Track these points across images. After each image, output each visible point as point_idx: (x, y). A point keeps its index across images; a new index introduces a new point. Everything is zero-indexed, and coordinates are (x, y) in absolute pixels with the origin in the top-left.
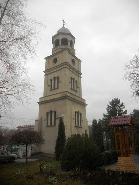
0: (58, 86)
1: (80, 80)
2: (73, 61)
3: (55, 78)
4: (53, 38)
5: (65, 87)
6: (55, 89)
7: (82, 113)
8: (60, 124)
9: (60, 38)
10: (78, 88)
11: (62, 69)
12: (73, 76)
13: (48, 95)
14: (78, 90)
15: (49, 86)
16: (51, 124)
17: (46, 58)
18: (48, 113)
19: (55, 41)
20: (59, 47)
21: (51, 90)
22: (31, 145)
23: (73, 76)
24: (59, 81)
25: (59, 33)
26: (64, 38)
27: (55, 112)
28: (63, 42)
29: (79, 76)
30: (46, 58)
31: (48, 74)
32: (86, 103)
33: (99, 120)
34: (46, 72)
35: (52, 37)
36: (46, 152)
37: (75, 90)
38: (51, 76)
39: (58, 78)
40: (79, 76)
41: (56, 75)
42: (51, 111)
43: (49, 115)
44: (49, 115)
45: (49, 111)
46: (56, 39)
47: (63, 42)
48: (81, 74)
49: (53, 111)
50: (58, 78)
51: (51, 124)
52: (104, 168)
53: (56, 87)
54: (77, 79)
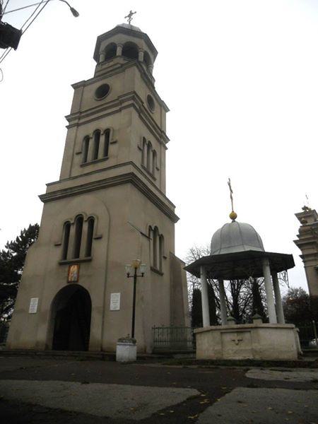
0: (89, 252)
1: (162, 154)
2: (150, 100)
4: (101, 39)
5: (125, 154)
6: (96, 159)
7: (158, 153)
8: (127, 29)
9: (121, 39)
12: (150, 138)
13: (73, 175)
14: (157, 176)
15: (78, 154)
16: (77, 254)
17: (75, 86)
20: (116, 61)
21: (85, 164)
23: (150, 138)
24: (110, 141)
25: (119, 30)
26: (127, 42)
28: (125, 53)
30: (75, 86)
31: (78, 125)
32: (177, 212)
34: (75, 119)
36: (52, 335)
37: (158, 268)
38: (89, 129)
39: (107, 132)
40: (161, 143)
41: (103, 124)
44: (91, 142)
46: (107, 44)
47: (125, 53)
48: (167, 140)
50: (107, 132)
51: (77, 254)
52: (201, 276)
53: (101, 156)
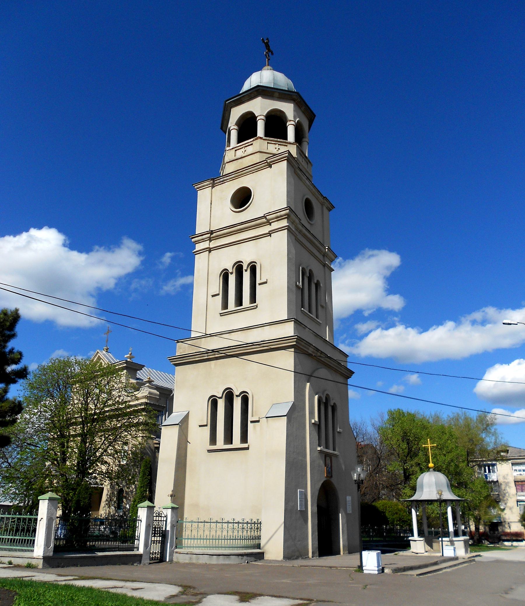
3: (239, 268)
10: (322, 307)
11: (269, 234)
18: (214, 402)
19: (98, 254)
22: (140, 474)
26: (485, 351)
27: (245, 400)
29: (324, 265)
33: (435, 545)
35: (315, 116)
40: (324, 265)
41: (246, 254)
42: (229, 396)
43: (232, 279)
44: (232, 279)
45: (229, 266)
46: (78, 258)
49: (236, 392)
54: (318, 275)
